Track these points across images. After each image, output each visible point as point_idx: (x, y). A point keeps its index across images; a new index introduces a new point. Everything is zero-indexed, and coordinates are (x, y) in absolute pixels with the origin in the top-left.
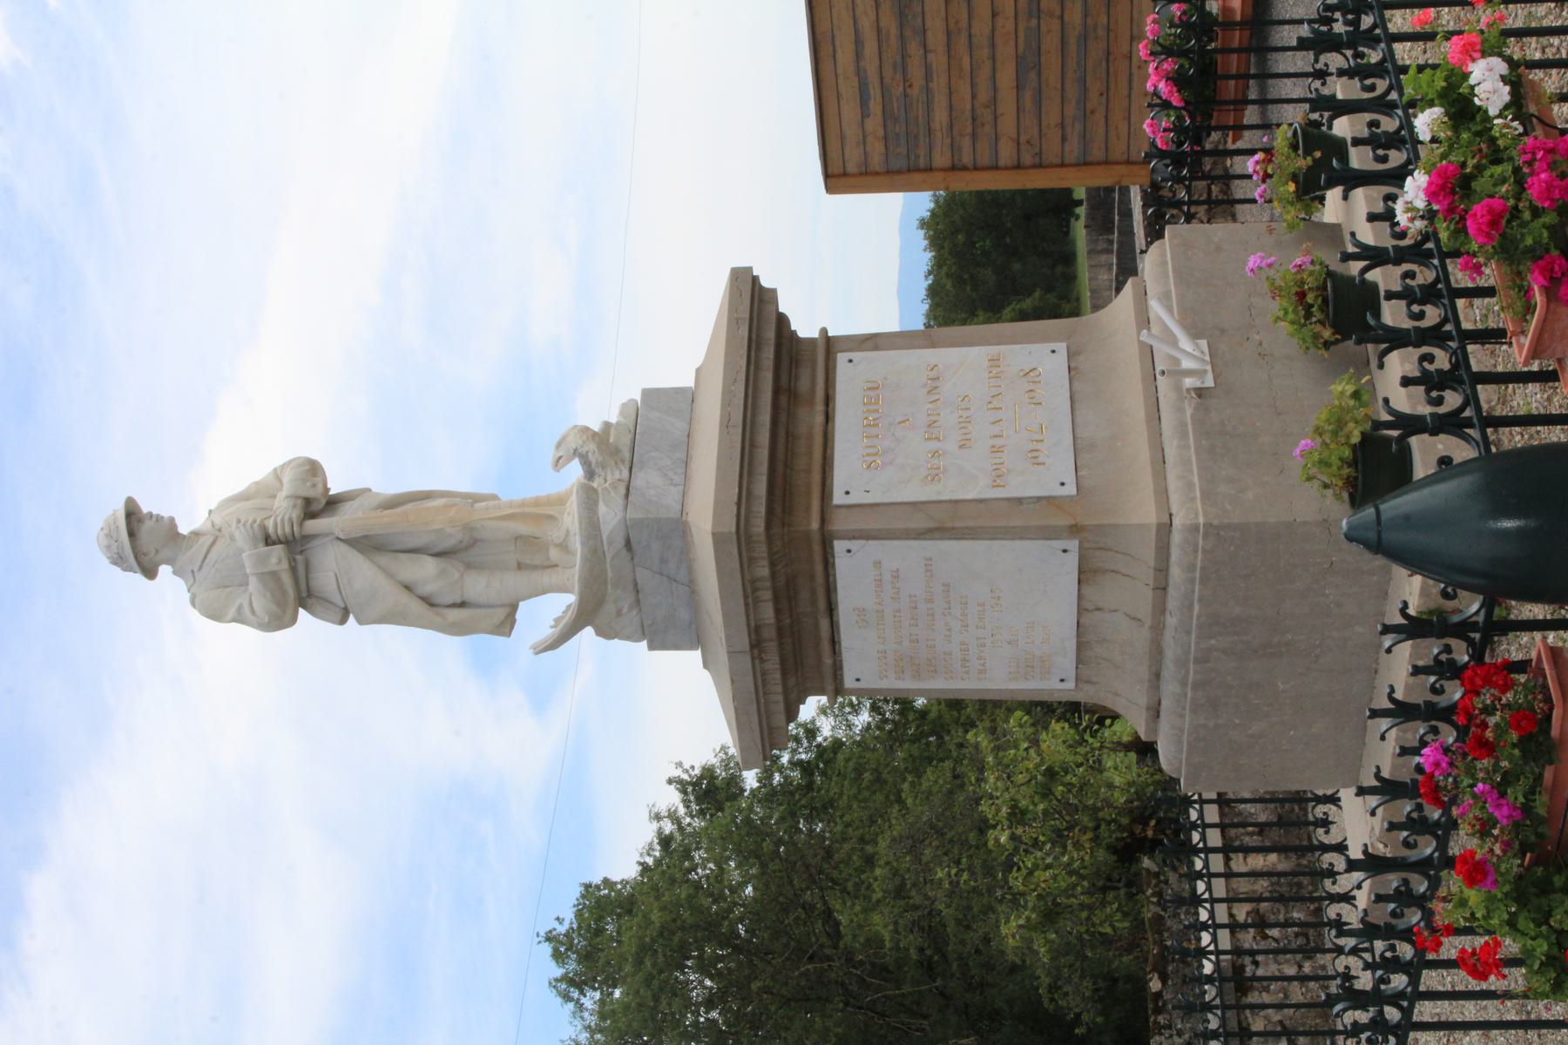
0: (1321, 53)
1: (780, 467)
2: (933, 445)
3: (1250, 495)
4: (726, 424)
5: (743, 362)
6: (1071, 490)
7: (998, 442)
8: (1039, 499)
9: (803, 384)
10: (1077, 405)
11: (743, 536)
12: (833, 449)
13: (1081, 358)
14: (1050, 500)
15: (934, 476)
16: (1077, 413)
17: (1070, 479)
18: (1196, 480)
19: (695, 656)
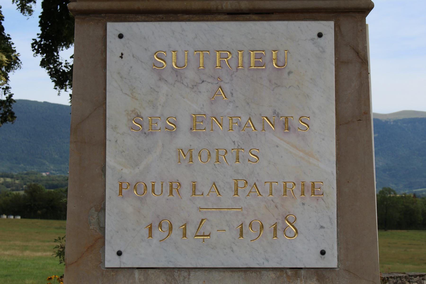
2: (185, 123)
7: (186, 190)
8: (103, 229)
14: (100, 240)
15: (140, 124)
17: (127, 261)
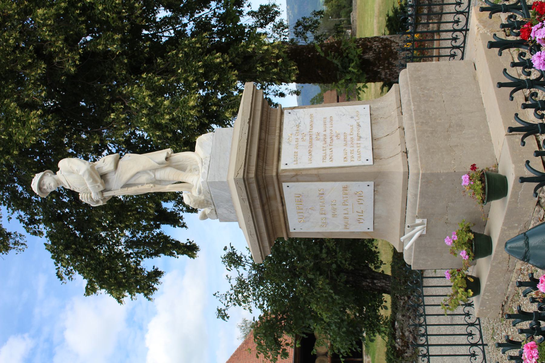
0: (494, 13)
1: (270, 228)
2: (323, 216)
3: (429, 263)
4: (242, 200)
5: (250, 215)
6: (371, 230)
9: (271, 192)
10: (376, 204)
11: (246, 180)
12: (287, 220)
13: (379, 187)
16: (376, 206)
18: (413, 254)
19: (236, 224)
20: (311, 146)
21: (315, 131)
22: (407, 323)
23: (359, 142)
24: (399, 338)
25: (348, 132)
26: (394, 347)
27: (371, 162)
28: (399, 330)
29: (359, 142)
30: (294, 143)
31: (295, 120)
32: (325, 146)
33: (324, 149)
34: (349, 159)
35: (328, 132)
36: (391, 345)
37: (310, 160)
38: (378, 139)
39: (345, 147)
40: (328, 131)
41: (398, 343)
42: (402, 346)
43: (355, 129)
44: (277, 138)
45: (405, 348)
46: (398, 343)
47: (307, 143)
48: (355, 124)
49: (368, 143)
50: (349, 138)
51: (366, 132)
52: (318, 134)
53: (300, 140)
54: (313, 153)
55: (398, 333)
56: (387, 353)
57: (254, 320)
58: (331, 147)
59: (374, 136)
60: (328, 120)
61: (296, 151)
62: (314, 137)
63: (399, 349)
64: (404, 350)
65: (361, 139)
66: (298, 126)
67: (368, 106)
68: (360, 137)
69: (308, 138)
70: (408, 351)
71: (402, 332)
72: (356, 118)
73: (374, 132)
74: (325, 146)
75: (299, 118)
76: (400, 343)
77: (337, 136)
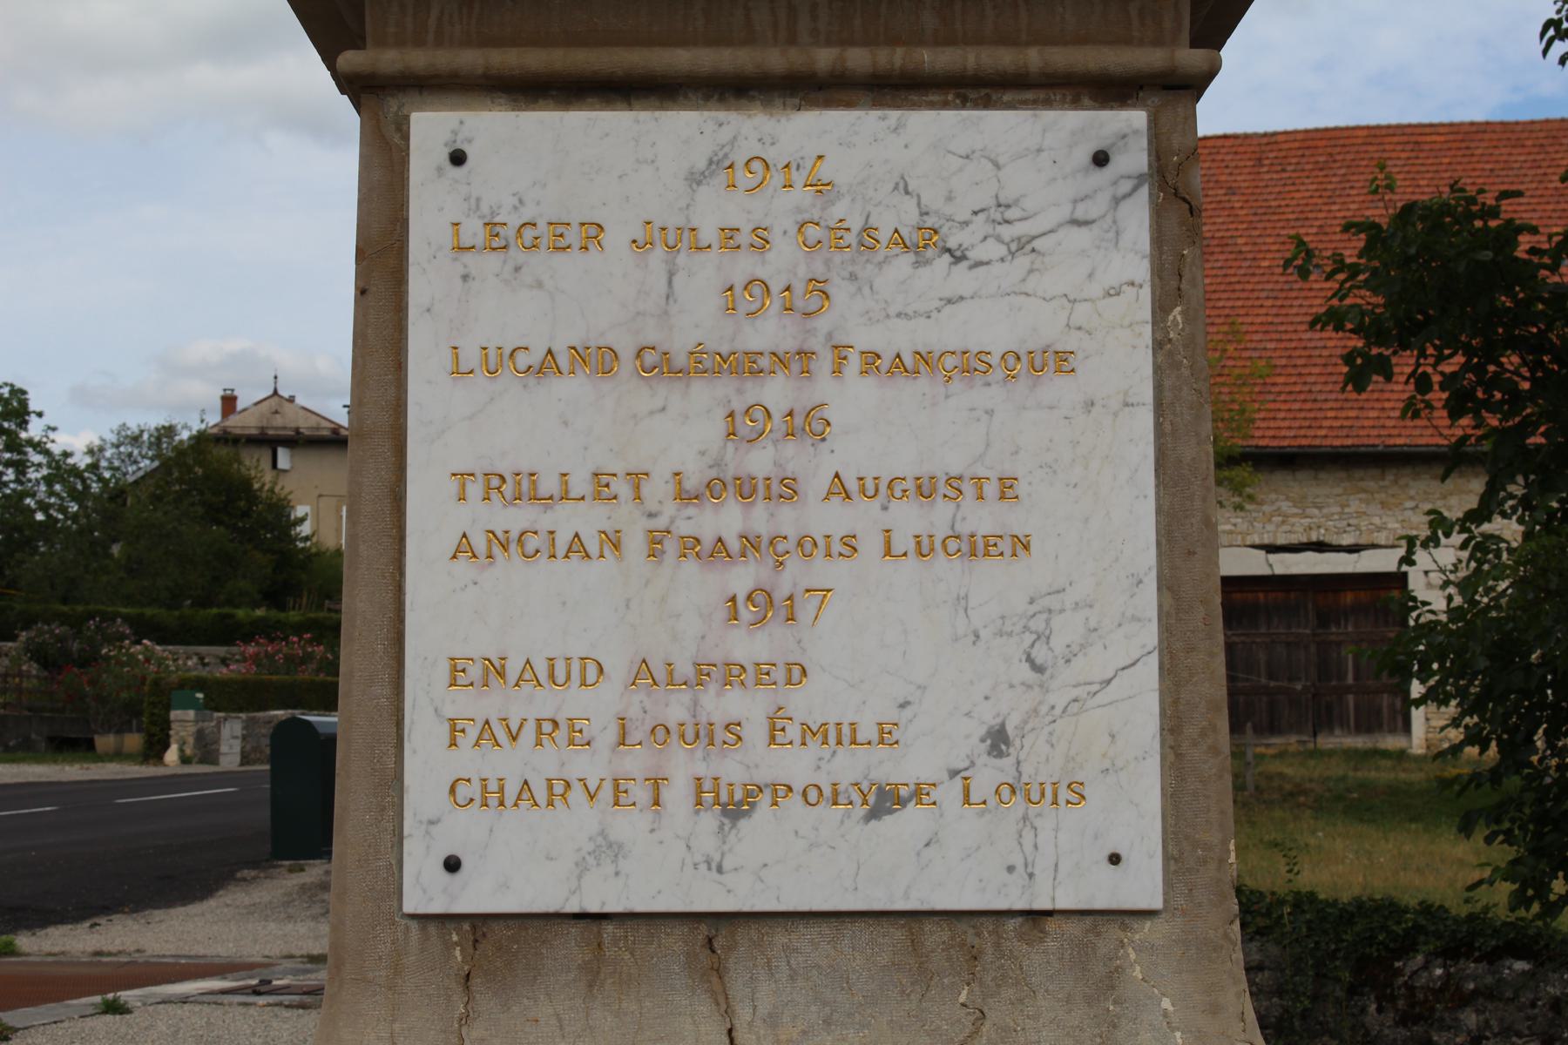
20: (658, 365)
21: (850, 399)
22: (1523, 1027)
23: (677, 794)
24: (1448, 975)
25: (805, 703)
26: (1407, 946)
27: (425, 890)
28: (1489, 980)
29: (677, 794)
30: (714, 210)
31: (1002, 209)
32: (658, 490)
33: (622, 488)
34: (470, 705)
35: (824, 518)
36: (1418, 928)
37: (498, 361)
38: (719, 971)
39: (618, 667)
40: (828, 519)
41: (1426, 966)
42: (1411, 989)
43: (847, 767)
44: (775, 59)
45: (1401, 1003)
46: (1426, 966)
47: (698, 321)
48: (903, 769)
49: (660, 873)
50: (745, 706)
51: (790, 863)
52: (808, 425)
53: (744, 266)
54: (572, 388)
55: (1473, 973)
56: (1389, 909)
57: (1505, 195)
58: (635, 543)
59: (746, 934)
60: (981, 519)
61: (617, 238)
62: (777, 393)
63: (1399, 972)
64: (1393, 999)
65: (710, 820)
66: (925, 242)
67: (1152, 898)
68: (735, 810)
69: (768, 333)
70: (1390, 1017)
71: (1476, 993)
72: (988, 775)
73: (805, 935)
74: (658, 490)
75: (1023, 245)
76: (1422, 980)
77: (767, 605)
